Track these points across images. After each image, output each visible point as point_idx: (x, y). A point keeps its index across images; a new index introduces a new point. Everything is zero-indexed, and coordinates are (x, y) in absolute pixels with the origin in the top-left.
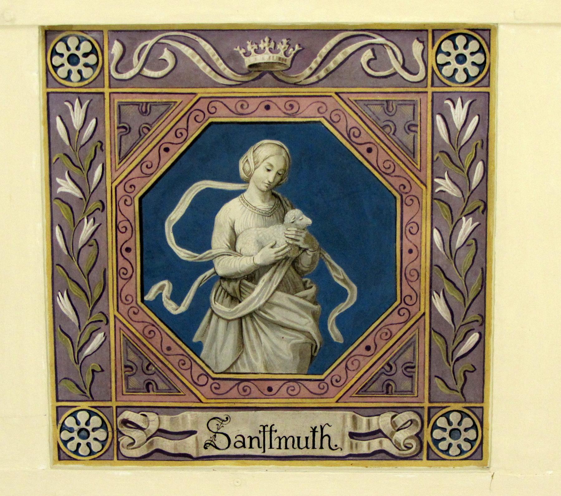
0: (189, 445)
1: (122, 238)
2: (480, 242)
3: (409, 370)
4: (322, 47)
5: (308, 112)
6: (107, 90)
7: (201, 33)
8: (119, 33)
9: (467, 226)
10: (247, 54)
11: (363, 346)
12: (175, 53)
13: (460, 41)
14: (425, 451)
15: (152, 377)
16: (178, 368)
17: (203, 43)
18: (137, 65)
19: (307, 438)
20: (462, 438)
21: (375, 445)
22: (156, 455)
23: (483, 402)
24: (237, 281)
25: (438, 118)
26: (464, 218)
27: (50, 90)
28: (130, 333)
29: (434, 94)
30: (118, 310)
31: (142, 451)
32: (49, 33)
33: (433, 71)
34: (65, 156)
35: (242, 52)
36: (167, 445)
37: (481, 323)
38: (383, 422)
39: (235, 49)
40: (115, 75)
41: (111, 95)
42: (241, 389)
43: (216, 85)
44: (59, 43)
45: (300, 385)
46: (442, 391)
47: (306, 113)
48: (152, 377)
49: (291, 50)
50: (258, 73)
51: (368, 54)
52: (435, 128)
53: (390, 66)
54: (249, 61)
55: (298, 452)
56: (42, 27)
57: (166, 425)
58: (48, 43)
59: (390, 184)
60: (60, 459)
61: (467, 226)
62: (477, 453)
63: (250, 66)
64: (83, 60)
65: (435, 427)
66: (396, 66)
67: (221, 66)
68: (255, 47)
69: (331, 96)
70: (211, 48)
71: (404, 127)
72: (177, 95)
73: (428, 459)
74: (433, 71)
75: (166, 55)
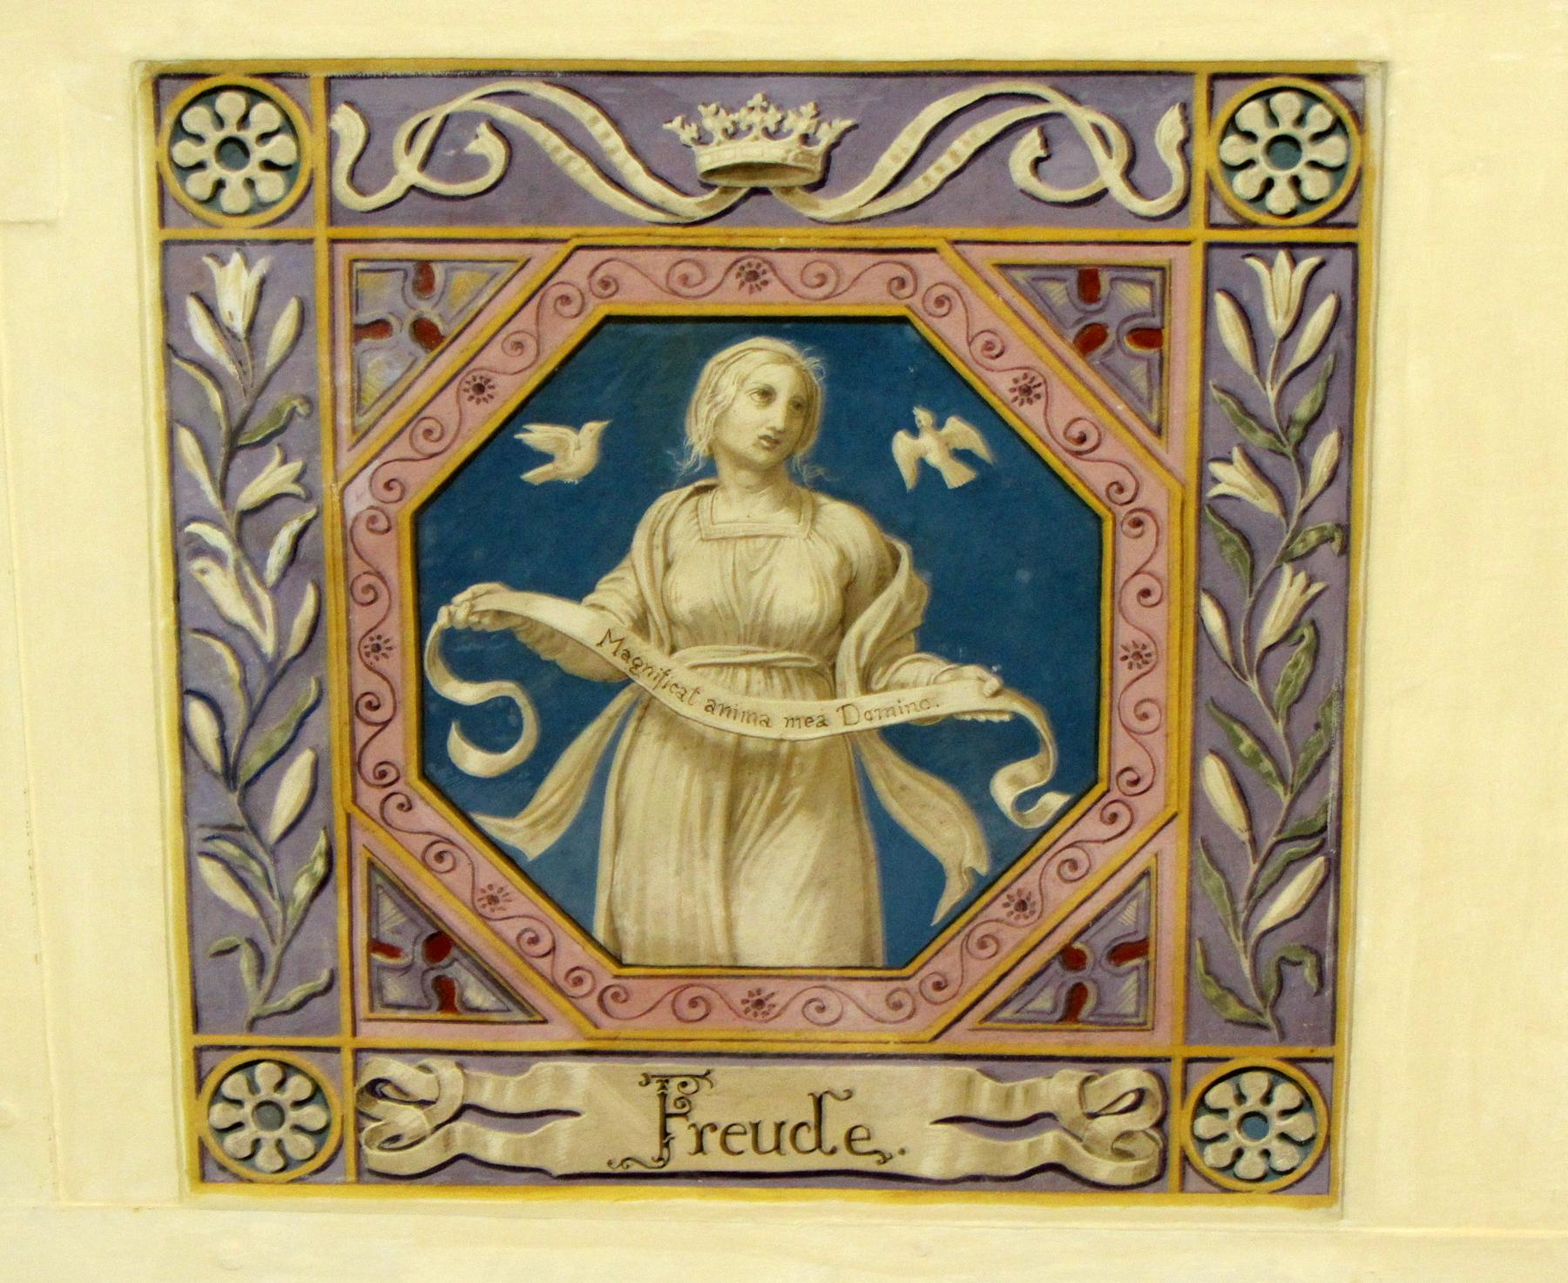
2: (1326, 637)
4: (883, 147)
7: (585, 84)
9: (1289, 593)
10: (703, 139)
12: (497, 128)
17: (584, 112)
20: (1272, 1133)
21: (1048, 1145)
22: (460, 1170)
23: (1333, 1041)
24: (946, 633)
25: (1223, 305)
26: (1287, 570)
31: (426, 1155)
34: (224, 419)
35: (688, 134)
36: (496, 1145)
37: (1323, 839)
38: (1057, 1089)
40: (349, 198)
42: (702, 1011)
44: (272, 1066)
46: (1228, 1043)
51: (1029, 145)
52: (1211, 331)
53: (1093, 171)
57: (485, 1097)
59: (1091, 478)
60: (203, 1177)
61: (1289, 593)
62: (1312, 1173)
64: (259, 153)
65: (1201, 1106)
66: (1110, 174)
67: (632, 170)
68: (726, 120)
69: (933, 250)
70: (588, 167)
75: (487, 145)
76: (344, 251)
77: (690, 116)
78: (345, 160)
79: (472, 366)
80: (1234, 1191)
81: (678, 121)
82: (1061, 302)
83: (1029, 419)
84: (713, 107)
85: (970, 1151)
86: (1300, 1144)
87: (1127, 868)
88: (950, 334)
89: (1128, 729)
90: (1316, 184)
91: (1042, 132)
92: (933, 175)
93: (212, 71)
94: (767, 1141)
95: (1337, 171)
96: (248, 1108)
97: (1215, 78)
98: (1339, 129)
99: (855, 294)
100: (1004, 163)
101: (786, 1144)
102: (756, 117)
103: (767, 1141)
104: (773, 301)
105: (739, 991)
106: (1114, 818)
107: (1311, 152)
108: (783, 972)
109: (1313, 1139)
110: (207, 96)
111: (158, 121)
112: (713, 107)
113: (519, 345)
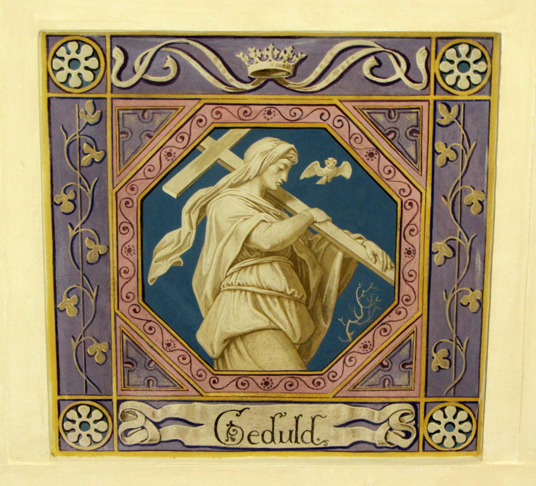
0: (190, 437)
1: (123, 239)
3: (407, 367)
5: (312, 119)
6: (109, 96)
8: (117, 38)
11: (359, 344)
13: (463, 49)
14: (418, 443)
15: (152, 373)
16: (178, 363)
18: (140, 70)
19: (291, 432)
27: (51, 95)
28: (125, 332)
29: (427, 102)
30: (118, 309)
32: (50, 39)
33: (436, 81)
39: (238, 56)
41: (114, 101)
43: (214, 91)
45: (298, 380)
46: (443, 387)
47: (308, 119)
48: (152, 373)
49: (295, 57)
50: (266, 79)
51: (371, 62)
54: (252, 69)
55: (282, 446)
56: (41, 32)
58: (50, 48)
63: (253, 73)
66: (399, 73)
68: (259, 54)
71: (406, 133)
72: (465, 119)
73: (424, 450)
74: (436, 81)
75: (170, 63)
76: (117, 103)
77: (247, 53)
78: (116, 68)
79: (180, 131)
80: (441, 451)
81: (241, 54)
82: (383, 120)
83: (371, 166)
84: (254, 49)
85: (345, 437)
86: (314, 418)
87: (154, 352)
88: (342, 134)
89: (406, 281)
90: (476, 79)
91: (376, 58)
92: (331, 77)
93: (46, 71)
94: (285, 437)
95: (483, 74)
96: (77, 424)
97: (438, 39)
98: (483, 58)
99: (308, 119)
100: (361, 69)
101: (299, 440)
102: (269, 53)
103: (285, 437)
104: (275, 120)
105: (259, 380)
106: (400, 313)
107: (474, 67)
108: (275, 373)
109: (471, 432)
110: (65, 44)
111: (48, 52)
112: (254, 49)
113: (183, 138)
